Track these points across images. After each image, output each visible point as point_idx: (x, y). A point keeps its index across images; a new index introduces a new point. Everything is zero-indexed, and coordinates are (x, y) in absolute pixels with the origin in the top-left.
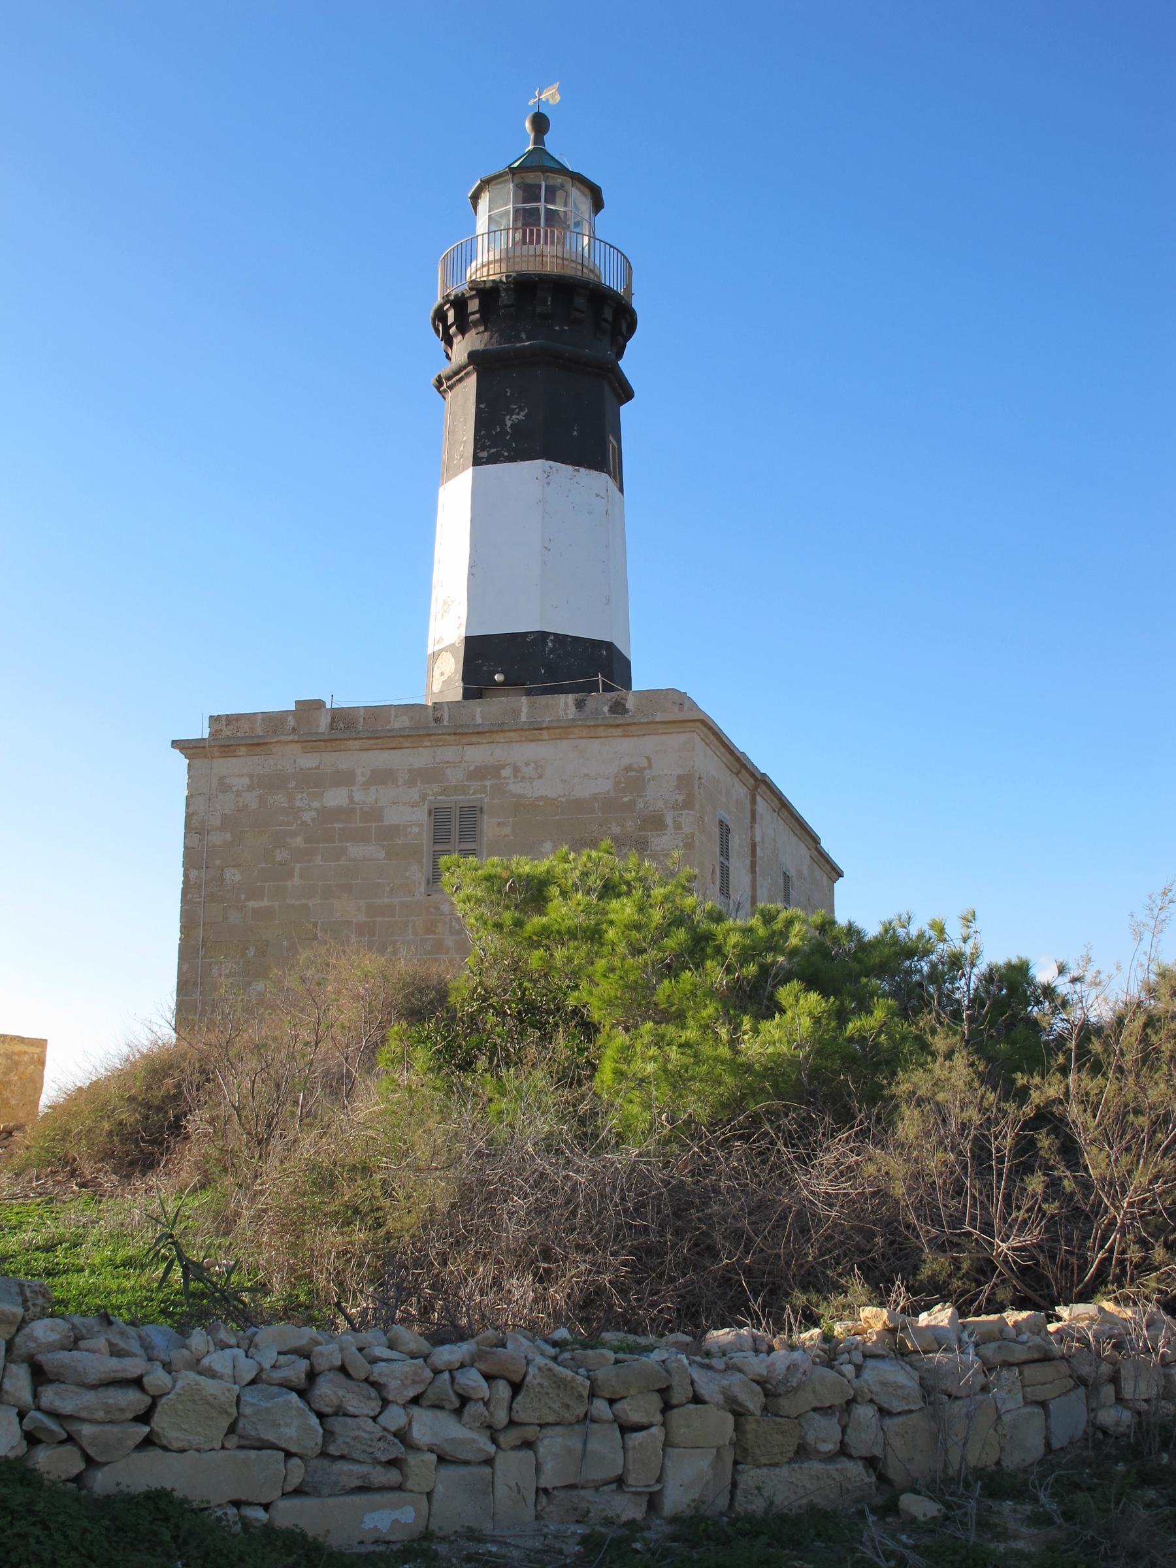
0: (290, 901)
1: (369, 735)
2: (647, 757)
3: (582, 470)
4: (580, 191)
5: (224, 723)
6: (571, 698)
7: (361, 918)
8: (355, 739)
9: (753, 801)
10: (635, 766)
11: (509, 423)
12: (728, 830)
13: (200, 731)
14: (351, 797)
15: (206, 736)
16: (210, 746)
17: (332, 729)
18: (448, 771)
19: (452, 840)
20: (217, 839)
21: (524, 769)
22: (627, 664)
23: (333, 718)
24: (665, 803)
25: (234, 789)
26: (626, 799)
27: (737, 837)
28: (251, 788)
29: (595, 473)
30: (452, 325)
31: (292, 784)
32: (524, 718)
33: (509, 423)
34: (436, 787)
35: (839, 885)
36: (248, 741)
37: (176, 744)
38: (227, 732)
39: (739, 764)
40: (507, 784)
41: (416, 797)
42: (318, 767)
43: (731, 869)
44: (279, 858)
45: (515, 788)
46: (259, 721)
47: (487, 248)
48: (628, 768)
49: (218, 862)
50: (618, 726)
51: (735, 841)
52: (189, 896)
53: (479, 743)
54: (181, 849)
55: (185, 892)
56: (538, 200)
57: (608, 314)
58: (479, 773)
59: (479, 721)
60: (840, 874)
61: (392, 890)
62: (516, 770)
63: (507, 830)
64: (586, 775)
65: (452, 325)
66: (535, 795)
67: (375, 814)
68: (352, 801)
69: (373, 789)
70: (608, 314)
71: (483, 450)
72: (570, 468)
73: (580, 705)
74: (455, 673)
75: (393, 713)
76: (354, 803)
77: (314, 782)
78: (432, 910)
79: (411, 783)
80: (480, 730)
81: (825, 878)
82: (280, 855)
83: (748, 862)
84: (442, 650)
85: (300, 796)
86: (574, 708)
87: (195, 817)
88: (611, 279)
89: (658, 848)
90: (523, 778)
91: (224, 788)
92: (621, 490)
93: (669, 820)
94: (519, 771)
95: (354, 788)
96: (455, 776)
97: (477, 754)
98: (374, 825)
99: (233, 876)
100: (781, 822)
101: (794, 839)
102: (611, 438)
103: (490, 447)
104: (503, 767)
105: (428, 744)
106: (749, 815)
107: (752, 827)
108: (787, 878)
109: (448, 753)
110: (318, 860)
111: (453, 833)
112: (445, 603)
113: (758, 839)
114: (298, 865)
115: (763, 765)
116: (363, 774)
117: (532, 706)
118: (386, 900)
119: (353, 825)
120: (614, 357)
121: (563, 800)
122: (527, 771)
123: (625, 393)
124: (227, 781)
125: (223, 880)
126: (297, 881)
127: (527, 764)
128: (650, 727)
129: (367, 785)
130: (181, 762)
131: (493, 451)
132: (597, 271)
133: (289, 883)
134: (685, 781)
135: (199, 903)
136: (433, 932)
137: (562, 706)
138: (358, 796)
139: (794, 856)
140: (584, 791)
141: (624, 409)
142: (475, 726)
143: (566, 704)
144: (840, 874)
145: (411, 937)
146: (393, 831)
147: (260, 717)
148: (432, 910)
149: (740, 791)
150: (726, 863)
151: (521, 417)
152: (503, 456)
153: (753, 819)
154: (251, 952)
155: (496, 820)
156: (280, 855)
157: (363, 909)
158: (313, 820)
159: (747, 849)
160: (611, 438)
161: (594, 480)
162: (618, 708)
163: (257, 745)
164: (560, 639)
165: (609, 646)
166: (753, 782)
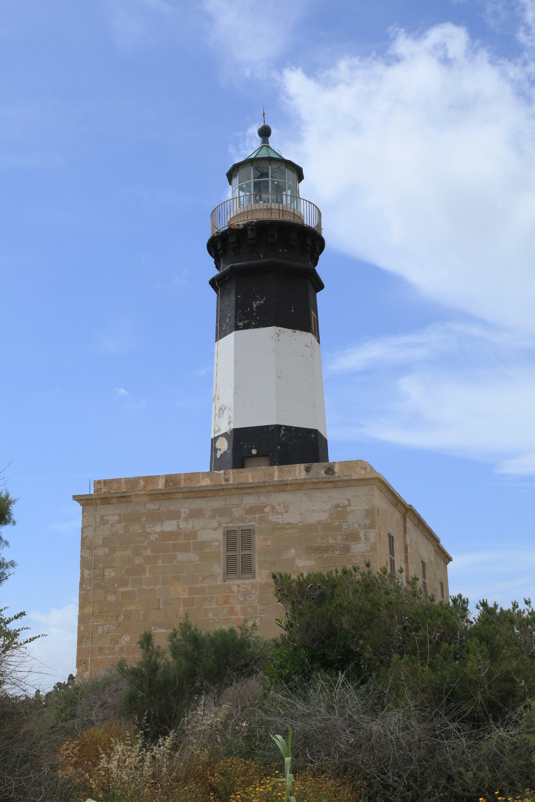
0: (144, 587)
1: (189, 490)
2: (348, 500)
3: (297, 331)
4: (290, 170)
5: (103, 484)
6: (302, 466)
7: (186, 596)
8: (180, 493)
9: (405, 521)
10: (341, 504)
11: (255, 306)
12: (393, 539)
13: (87, 490)
14: (178, 526)
15: (92, 492)
16: (95, 499)
17: (166, 486)
18: (234, 510)
19: (237, 549)
20: (100, 552)
21: (277, 508)
22: (325, 441)
23: (166, 481)
24: (359, 525)
25: (110, 522)
26: (336, 524)
27: (397, 543)
28: (119, 522)
29: (304, 333)
30: (220, 250)
31: (144, 519)
32: (276, 478)
33: (255, 306)
34: (227, 519)
35: (450, 566)
36: (118, 495)
37: (77, 498)
38: (104, 490)
39: (396, 501)
40: (268, 516)
41: (216, 525)
42: (158, 509)
43: (395, 561)
44: (137, 562)
45: (273, 518)
46: (123, 483)
47: (234, 203)
48: (337, 506)
49: (101, 566)
50: (330, 482)
51: (398, 545)
52: (84, 586)
53: (251, 493)
54: (79, 559)
55: (82, 584)
56: (268, 177)
57: (309, 242)
58: (252, 510)
59: (250, 480)
60: (450, 560)
61: (204, 578)
62: (273, 508)
63: (269, 543)
64: (313, 510)
65: (220, 250)
66: (285, 522)
67: (192, 535)
68: (179, 528)
69: (191, 521)
70: (309, 242)
71: (240, 321)
72: (290, 330)
73: (308, 470)
74: (228, 449)
75: (201, 477)
76: (181, 529)
77: (157, 517)
78: (227, 590)
79: (212, 517)
80: (252, 485)
81: (442, 563)
82: (138, 560)
83: (403, 557)
84: (219, 436)
85: (148, 526)
86: (305, 472)
87: (87, 539)
88: (309, 221)
89: (356, 551)
90: (277, 513)
91: (104, 522)
92: (319, 342)
93: (362, 535)
94: (275, 509)
95: (179, 520)
96: (238, 512)
97: (250, 501)
98: (192, 541)
99: (110, 573)
100: (419, 532)
101: (426, 541)
102: (313, 313)
103: (244, 320)
104: (265, 506)
105: (222, 494)
106: (402, 529)
107: (404, 536)
108: (423, 564)
109: (234, 500)
110: (160, 563)
111: (237, 545)
112: (221, 409)
113: (408, 543)
114: (149, 566)
115: (408, 500)
116: (185, 512)
117: (281, 471)
118: (200, 585)
119: (180, 542)
120: (312, 266)
121: (301, 524)
122: (279, 509)
123: (319, 286)
124: (106, 518)
125: (103, 575)
126: (148, 575)
127: (279, 505)
128: (349, 483)
129: (187, 518)
130: (78, 508)
131: (246, 322)
132: (302, 218)
133: (143, 577)
134: (370, 513)
135: (90, 590)
136: (228, 603)
137: (298, 471)
138: (183, 525)
139: (426, 551)
140: (312, 519)
141: (319, 295)
142: (248, 483)
143: (300, 470)
144: (450, 560)
145: (215, 606)
146: (203, 544)
147: (123, 481)
148: (227, 590)
149: (397, 516)
150: (393, 558)
151: (261, 302)
152: (252, 324)
153: (405, 531)
154: (121, 618)
155: (262, 537)
156: (138, 560)
157: (187, 590)
158: (156, 539)
159: (403, 549)
160: (313, 313)
161: (304, 337)
162: (330, 470)
163: (123, 498)
164: (289, 429)
165: (316, 432)
166: (404, 510)
